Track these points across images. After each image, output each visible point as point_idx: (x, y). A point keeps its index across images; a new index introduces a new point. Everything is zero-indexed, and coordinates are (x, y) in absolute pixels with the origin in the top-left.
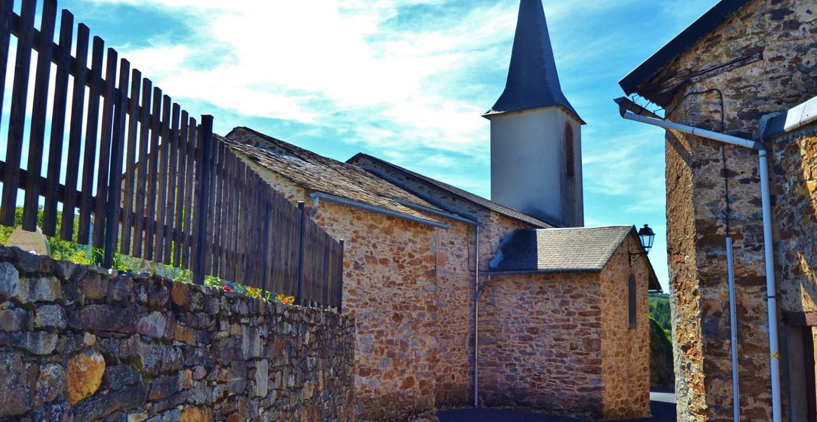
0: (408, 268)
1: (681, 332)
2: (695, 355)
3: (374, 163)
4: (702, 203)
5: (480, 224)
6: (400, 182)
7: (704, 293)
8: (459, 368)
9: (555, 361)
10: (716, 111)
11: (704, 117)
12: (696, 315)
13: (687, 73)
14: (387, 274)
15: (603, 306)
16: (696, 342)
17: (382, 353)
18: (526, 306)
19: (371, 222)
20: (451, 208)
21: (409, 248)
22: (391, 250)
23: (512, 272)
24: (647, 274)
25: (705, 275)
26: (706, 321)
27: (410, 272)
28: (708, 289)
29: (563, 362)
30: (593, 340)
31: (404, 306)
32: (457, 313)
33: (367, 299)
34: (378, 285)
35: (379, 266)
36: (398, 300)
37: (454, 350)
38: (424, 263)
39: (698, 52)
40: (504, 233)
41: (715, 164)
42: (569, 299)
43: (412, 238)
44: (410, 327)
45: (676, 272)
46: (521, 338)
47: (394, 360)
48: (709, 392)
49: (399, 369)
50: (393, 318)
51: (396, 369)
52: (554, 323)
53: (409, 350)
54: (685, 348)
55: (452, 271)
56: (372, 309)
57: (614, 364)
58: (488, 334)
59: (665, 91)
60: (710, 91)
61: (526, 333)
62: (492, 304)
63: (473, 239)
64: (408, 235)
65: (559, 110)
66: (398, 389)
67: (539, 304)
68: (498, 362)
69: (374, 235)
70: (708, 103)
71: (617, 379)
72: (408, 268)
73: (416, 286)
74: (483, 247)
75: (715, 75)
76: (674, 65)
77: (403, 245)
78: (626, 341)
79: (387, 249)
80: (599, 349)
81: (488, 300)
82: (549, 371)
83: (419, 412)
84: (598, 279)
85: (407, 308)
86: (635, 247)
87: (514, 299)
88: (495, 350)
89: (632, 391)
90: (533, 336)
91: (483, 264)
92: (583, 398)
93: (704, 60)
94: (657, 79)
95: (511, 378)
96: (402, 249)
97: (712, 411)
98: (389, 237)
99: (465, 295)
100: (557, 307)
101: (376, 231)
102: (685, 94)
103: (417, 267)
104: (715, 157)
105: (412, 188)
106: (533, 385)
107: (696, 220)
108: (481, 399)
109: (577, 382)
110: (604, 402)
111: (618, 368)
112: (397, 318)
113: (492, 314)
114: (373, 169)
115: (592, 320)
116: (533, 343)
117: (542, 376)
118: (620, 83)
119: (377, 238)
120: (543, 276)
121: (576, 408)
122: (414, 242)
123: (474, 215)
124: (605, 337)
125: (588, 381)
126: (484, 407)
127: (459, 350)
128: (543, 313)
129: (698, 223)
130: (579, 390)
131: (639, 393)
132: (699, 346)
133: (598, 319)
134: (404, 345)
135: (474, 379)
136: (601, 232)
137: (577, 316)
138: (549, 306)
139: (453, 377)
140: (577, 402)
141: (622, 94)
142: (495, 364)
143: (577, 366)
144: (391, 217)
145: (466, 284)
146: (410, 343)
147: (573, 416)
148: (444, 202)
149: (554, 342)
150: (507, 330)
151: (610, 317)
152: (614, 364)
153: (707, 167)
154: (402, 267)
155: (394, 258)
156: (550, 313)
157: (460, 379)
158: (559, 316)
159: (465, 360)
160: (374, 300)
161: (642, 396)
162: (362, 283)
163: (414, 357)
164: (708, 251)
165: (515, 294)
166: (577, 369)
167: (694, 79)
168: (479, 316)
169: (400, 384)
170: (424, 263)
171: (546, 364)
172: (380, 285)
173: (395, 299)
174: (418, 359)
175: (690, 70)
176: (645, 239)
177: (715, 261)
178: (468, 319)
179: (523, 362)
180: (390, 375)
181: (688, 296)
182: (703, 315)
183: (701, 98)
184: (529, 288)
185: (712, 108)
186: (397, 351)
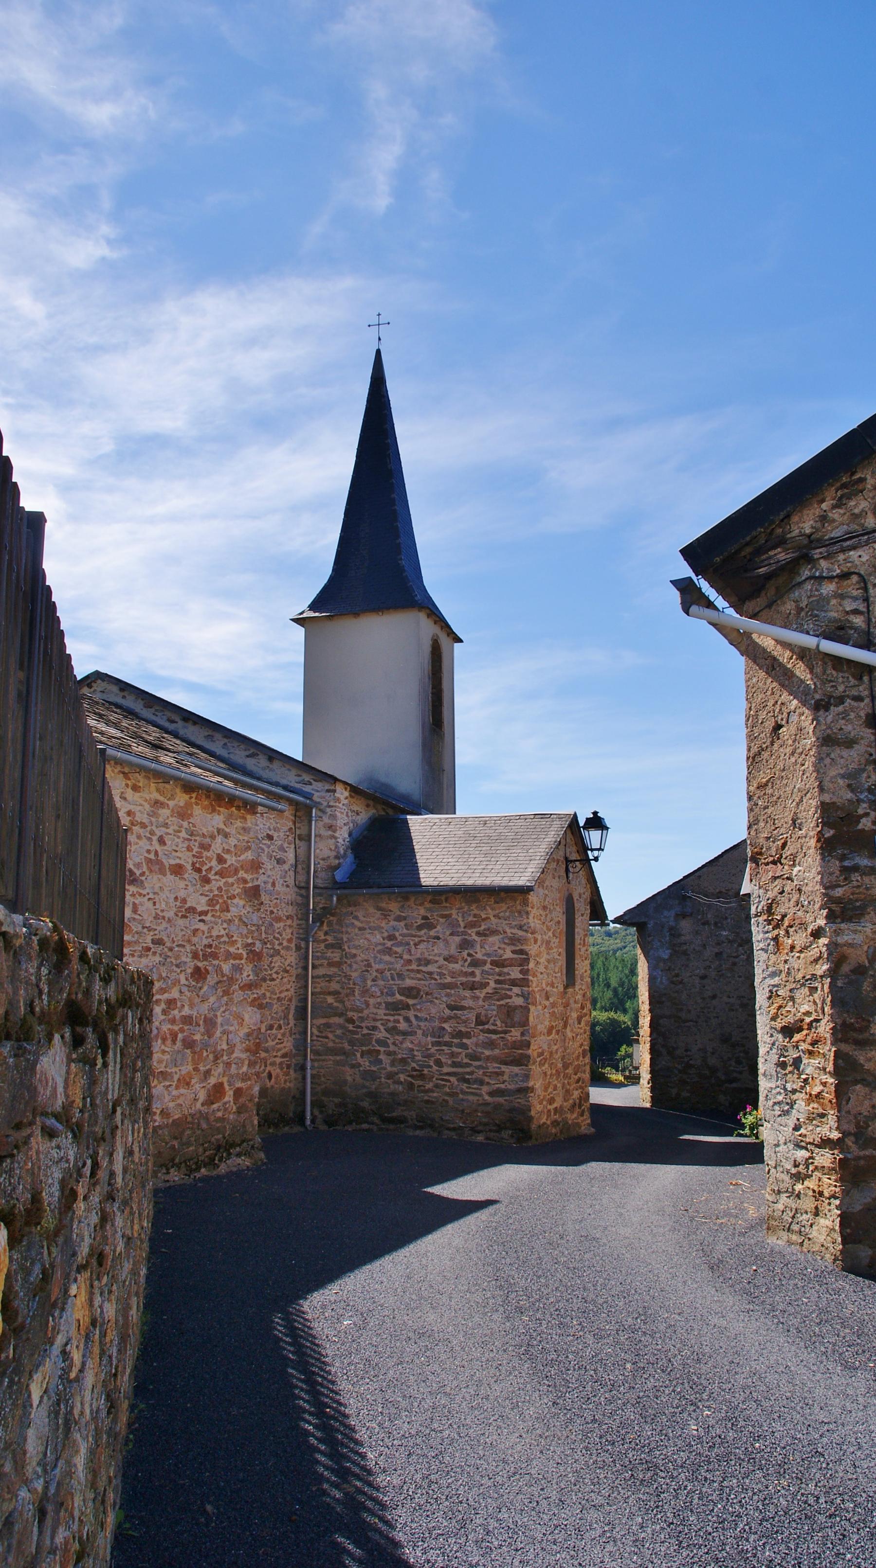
0: (217, 883)
1: (779, 1001)
2: (814, 1043)
3: (122, 690)
4: (833, 773)
5: (317, 804)
6: (171, 727)
7: (837, 933)
8: (278, 1060)
9: (447, 1044)
10: (856, 612)
11: (836, 620)
12: (820, 972)
13: (806, 541)
14: (182, 894)
15: (532, 949)
16: (817, 1021)
17: (174, 1041)
18: (399, 950)
19: (156, 796)
20: (265, 774)
21: (218, 846)
22: (189, 849)
23: (375, 890)
24: (588, 895)
25: (838, 901)
26: (839, 984)
27: (220, 889)
28: (843, 926)
29: (464, 1046)
30: (516, 1008)
31: (209, 953)
32: (277, 962)
33: (149, 939)
34: (167, 915)
35: (170, 877)
36: (201, 941)
37: (271, 1027)
38: (242, 874)
39: (824, 506)
40: (353, 822)
41: (855, 704)
42: (475, 937)
43: (222, 826)
44: (220, 992)
45: (770, 894)
46: (388, 1005)
47: (194, 1053)
48: (845, 1108)
49: (202, 1069)
50: (192, 975)
51: (196, 1069)
52: (449, 980)
53: (218, 1034)
54: (788, 1031)
55: (269, 886)
56: (157, 959)
57: (545, 1047)
58: (330, 999)
59: (762, 571)
60: (845, 576)
61: (398, 997)
62: (338, 946)
63: (303, 831)
64: (217, 820)
65: (422, 616)
66: (199, 1105)
67: (422, 946)
68: (346, 1046)
69: (161, 819)
70: (842, 597)
71: (549, 1073)
72: (217, 883)
73: (229, 916)
74: (321, 845)
75: (854, 548)
76: (779, 526)
77: (208, 840)
78: (561, 1008)
79: (183, 846)
80: (525, 1023)
81: (330, 940)
82: (439, 1063)
83: (233, 1145)
84: (525, 903)
85: (215, 956)
86: (574, 849)
87: (378, 938)
88: (341, 1026)
89: (567, 1091)
90: (411, 1002)
91: (322, 875)
92: (497, 1106)
93: (834, 521)
94: (749, 550)
95: (368, 1075)
96: (205, 847)
97: (849, 1142)
98: (185, 824)
99: (289, 931)
100: (453, 950)
101: (164, 813)
102: (799, 579)
103: (230, 880)
104: (854, 692)
105: (192, 738)
106: (411, 1086)
107: (822, 803)
108: (316, 1112)
109: (487, 1079)
110: (533, 1113)
111: (551, 1053)
112: (199, 974)
113: (338, 964)
114: (119, 700)
115: (515, 973)
116: (411, 1014)
117: (426, 1071)
118: (681, 551)
119: (166, 825)
120: (429, 898)
121: (486, 1124)
122: (226, 836)
123: (307, 789)
124: (534, 1004)
125: (506, 1077)
126: (323, 1127)
127: (280, 1027)
128: (428, 962)
129: (825, 808)
130: (491, 1094)
131: (576, 1094)
132: (825, 1028)
133: (525, 972)
134: (210, 1023)
135: (304, 1078)
136: (521, 822)
137: (488, 967)
138: (439, 949)
139: (270, 1076)
140: (487, 1114)
141: (685, 571)
142: (344, 1053)
143: (487, 1053)
144: (189, 787)
145: (291, 910)
146: (219, 1020)
147: (480, 1138)
148: (250, 764)
149: (447, 1012)
150: (365, 992)
151: (541, 968)
152: (545, 1047)
153: (841, 708)
154: (206, 880)
155: (193, 864)
156: (442, 961)
157: (283, 1080)
158: (456, 967)
159: (288, 1045)
160: (158, 942)
161: (580, 1098)
162: (141, 910)
163: (225, 1047)
164: (843, 858)
165: (379, 928)
166: (488, 1058)
167: (816, 553)
168: (314, 967)
169: (202, 1096)
170: (242, 874)
171: (433, 1050)
172: (170, 914)
173: (195, 940)
174: (231, 1048)
175: (809, 536)
176: (593, 837)
177: (855, 877)
178: (294, 972)
179: (392, 1048)
180: (185, 1082)
181: (800, 938)
182: (833, 973)
183: (828, 588)
184: (405, 918)
185: (849, 605)
186: (197, 1037)
